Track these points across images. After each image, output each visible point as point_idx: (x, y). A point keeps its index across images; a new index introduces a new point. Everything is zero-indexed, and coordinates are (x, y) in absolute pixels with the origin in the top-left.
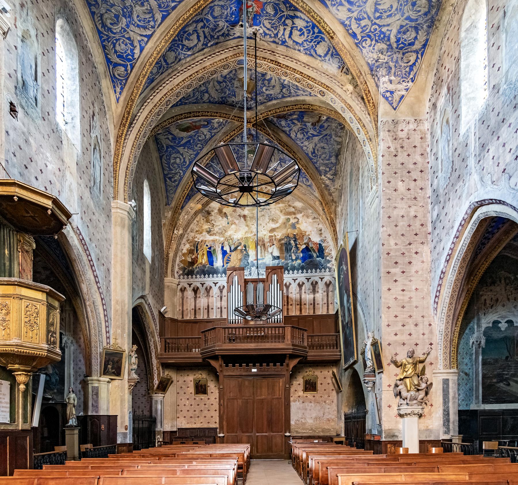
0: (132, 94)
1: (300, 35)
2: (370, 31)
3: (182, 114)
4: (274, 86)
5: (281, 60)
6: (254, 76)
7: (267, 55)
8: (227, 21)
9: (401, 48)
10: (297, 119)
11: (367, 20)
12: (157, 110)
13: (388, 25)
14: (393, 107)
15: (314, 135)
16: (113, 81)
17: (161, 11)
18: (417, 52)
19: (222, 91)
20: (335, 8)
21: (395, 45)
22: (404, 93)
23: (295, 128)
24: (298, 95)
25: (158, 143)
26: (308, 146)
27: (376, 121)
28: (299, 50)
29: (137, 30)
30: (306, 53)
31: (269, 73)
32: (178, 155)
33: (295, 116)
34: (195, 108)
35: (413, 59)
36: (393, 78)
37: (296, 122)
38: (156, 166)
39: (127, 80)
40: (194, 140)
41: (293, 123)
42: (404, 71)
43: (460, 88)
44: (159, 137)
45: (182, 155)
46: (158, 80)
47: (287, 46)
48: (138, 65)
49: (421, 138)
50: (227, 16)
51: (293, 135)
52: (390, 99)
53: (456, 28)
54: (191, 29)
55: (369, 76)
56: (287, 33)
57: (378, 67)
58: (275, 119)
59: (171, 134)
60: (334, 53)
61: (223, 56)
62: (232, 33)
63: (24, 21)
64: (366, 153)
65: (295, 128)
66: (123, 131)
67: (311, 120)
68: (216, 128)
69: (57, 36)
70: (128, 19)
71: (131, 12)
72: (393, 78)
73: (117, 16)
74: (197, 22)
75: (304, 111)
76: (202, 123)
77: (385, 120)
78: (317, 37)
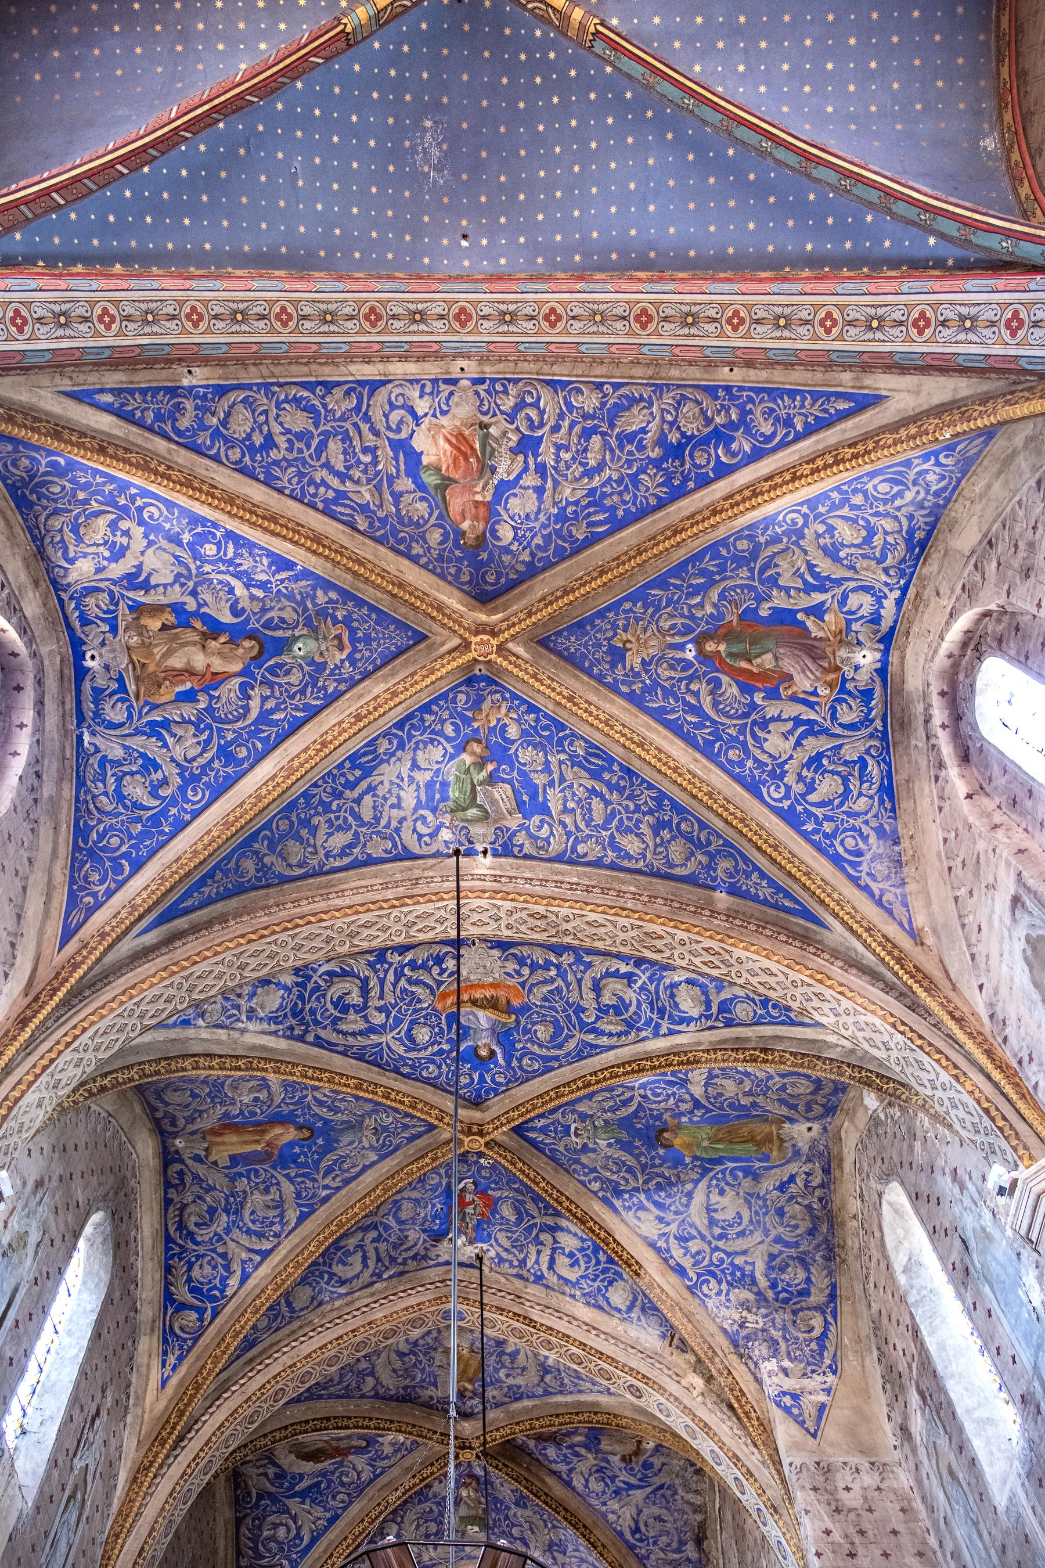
0: (200, 1372)
1: (572, 1265)
2: (712, 1264)
3: (307, 1422)
4: (524, 1369)
5: (535, 1314)
6: (478, 1344)
7: (507, 1303)
8: (424, 1231)
9: (786, 1301)
10: (586, 1446)
11: (698, 1241)
12: (251, 1410)
13: (745, 1253)
14: (807, 1430)
15: (631, 1487)
16: (165, 1341)
17: (299, 1205)
18: (820, 1309)
19: (407, 1373)
20: (631, 1213)
21: (770, 1294)
22: (822, 1398)
23: (583, 1467)
24: (580, 1392)
25: (237, 1486)
26: (622, 1513)
27: (778, 1464)
28: (573, 1296)
29: (245, 1240)
30: (588, 1303)
31: (512, 1340)
32: (284, 1518)
33: (578, 1439)
34: (339, 1407)
35: (817, 1322)
36: (786, 1363)
37: (583, 1451)
38: (221, 1544)
39: (196, 1340)
40: (330, 1481)
41: (577, 1455)
42: (807, 1350)
43: (946, 1394)
44: (243, 1469)
45: (295, 1518)
46: (266, 1344)
47: (547, 1287)
48: (228, 1309)
49: (903, 1510)
50: (425, 1220)
51: (578, 1483)
52: (795, 1411)
53: (883, 1266)
54: (351, 1242)
55: (733, 1358)
56: (545, 1259)
57: (747, 1338)
58: (532, 1443)
59: (275, 1465)
60: (646, 1306)
61: (413, 1301)
62: (432, 1254)
63: (27, 1216)
64: (773, 1542)
65: (583, 1467)
66: (156, 1456)
67: (618, 1448)
68: (387, 1457)
69: (82, 1244)
70: (233, 1218)
71: (242, 1205)
72: (786, 1363)
73: (212, 1211)
74: (366, 1229)
75: (598, 1429)
76: (354, 1443)
77: (797, 1462)
78: (605, 1271)
